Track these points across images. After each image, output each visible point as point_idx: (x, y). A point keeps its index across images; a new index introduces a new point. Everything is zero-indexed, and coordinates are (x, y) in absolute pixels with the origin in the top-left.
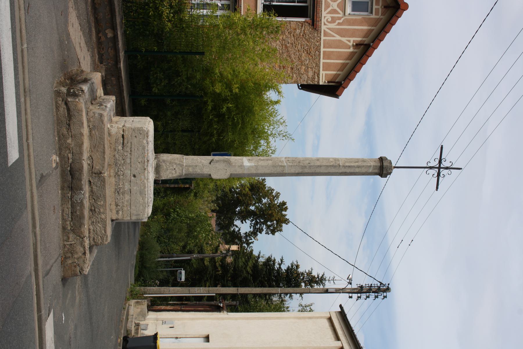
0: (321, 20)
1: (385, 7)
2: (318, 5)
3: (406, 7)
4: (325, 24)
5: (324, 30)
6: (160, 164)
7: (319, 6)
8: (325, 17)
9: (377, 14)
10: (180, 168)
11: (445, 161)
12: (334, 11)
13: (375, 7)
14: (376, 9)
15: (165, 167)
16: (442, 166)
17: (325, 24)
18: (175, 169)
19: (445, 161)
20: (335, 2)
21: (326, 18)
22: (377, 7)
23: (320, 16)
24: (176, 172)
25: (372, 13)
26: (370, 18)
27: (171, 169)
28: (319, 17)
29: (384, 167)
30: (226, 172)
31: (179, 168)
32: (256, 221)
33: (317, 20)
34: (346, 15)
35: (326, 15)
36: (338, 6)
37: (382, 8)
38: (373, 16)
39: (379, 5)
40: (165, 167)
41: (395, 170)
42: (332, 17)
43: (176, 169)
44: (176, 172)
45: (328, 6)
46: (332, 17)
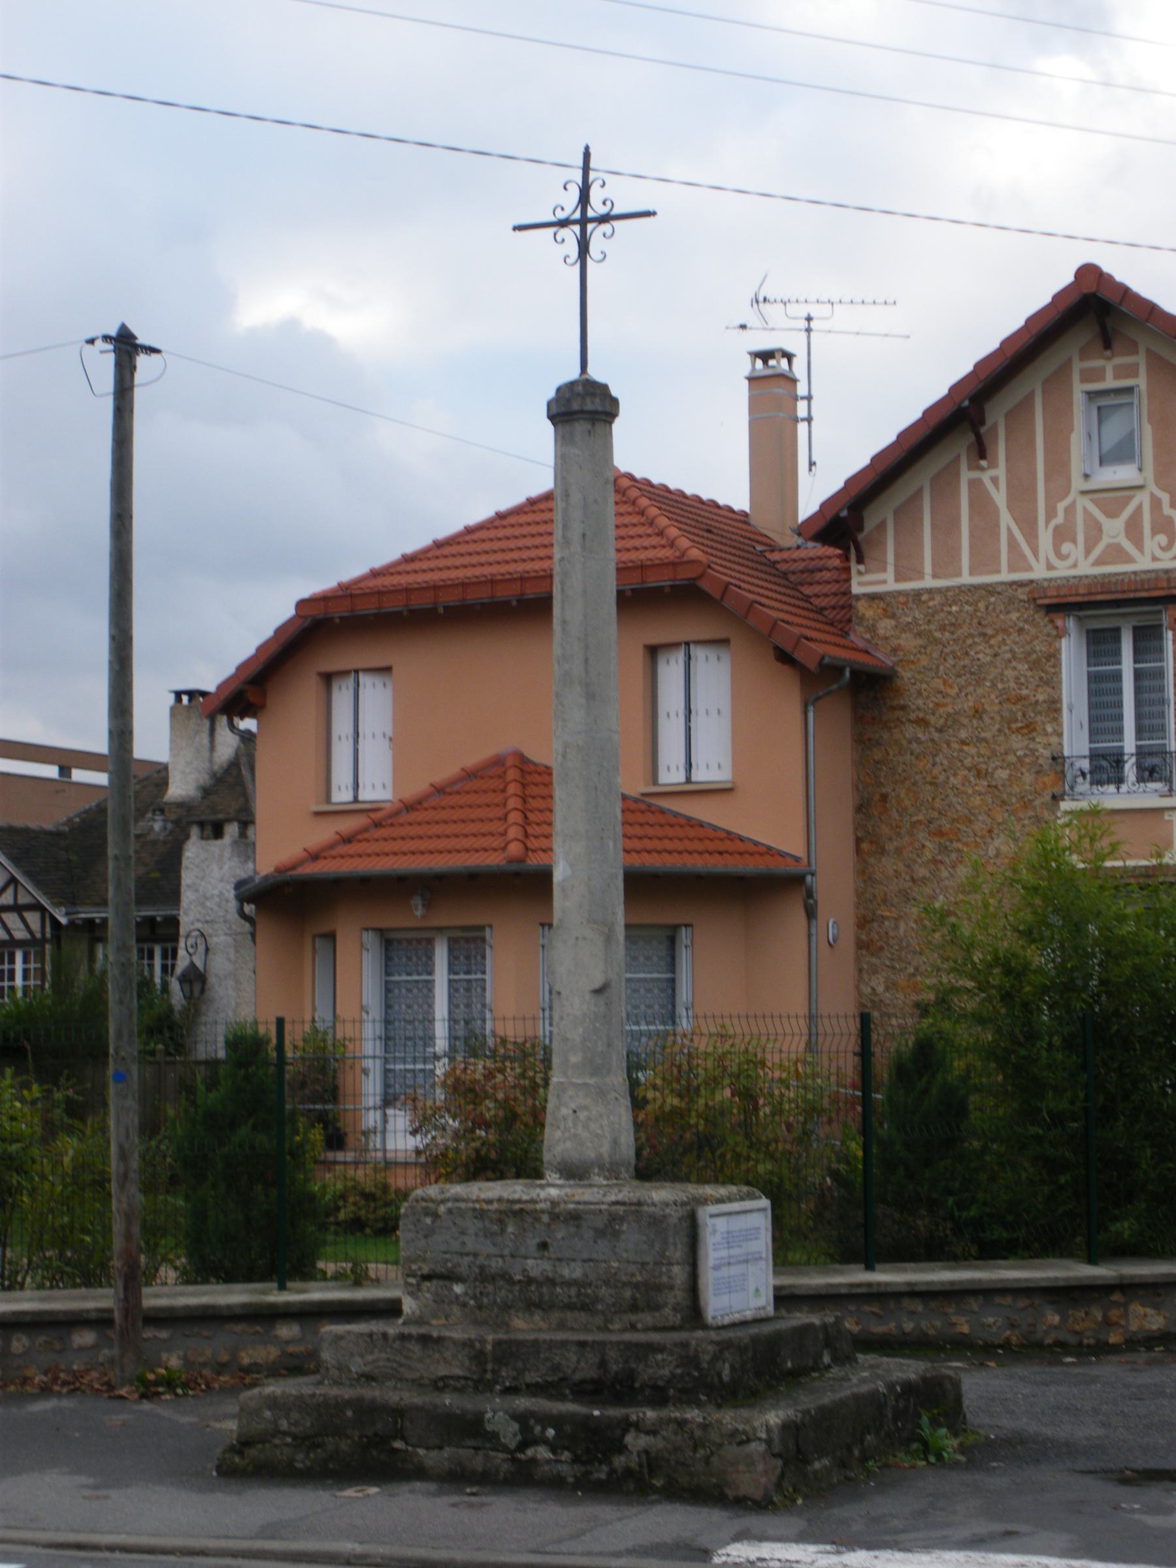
0: (1167, 571)
1: (1107, 344)
2: (1113, 589)
3: (1089, 273)
4: (1075, 566)
5: (1098, 562)
6: (558, 1159)
7: (1116, 583)
8: (1155, 559)
9: (1132, 371)
10: (570, 1093)
11: (563, 209)
12: (1133, 529)
13: (1110, 383)
14: (1117, 377)
15: (569, 1144)
16: (590, 214)
17: (1075, 566)
18: (575, 1112)
19: (563, 209)
20: (1100, 530)
21: (1159, 553)
22: (1109, 374)
23: (1153, 575)
24: (586, 1108)
25: (1129, 390)
26: (1151, 395)
27: (575, 1125)
28: (1157, 579)
29: (563, 409)
30: (585, 939)
31: (571, 1097)
32: (1071, 821)
33: (1165, 585)
34: (1140, 482)
35: (1148, 557)
36: (1112, 514)
37: (1113, 356)
38: (1141, 382)
39: (1103, 369)
40: (569, 1144)
41: (596, 373)
42: (1155, 532)
43: (573, 1106)
44: (586, 1108)
45: (1116, 553)
46: (1155, 532)
